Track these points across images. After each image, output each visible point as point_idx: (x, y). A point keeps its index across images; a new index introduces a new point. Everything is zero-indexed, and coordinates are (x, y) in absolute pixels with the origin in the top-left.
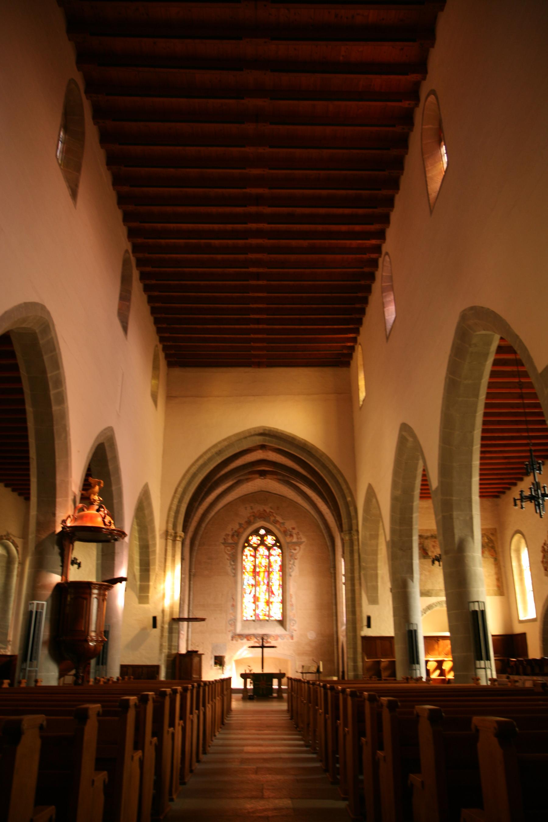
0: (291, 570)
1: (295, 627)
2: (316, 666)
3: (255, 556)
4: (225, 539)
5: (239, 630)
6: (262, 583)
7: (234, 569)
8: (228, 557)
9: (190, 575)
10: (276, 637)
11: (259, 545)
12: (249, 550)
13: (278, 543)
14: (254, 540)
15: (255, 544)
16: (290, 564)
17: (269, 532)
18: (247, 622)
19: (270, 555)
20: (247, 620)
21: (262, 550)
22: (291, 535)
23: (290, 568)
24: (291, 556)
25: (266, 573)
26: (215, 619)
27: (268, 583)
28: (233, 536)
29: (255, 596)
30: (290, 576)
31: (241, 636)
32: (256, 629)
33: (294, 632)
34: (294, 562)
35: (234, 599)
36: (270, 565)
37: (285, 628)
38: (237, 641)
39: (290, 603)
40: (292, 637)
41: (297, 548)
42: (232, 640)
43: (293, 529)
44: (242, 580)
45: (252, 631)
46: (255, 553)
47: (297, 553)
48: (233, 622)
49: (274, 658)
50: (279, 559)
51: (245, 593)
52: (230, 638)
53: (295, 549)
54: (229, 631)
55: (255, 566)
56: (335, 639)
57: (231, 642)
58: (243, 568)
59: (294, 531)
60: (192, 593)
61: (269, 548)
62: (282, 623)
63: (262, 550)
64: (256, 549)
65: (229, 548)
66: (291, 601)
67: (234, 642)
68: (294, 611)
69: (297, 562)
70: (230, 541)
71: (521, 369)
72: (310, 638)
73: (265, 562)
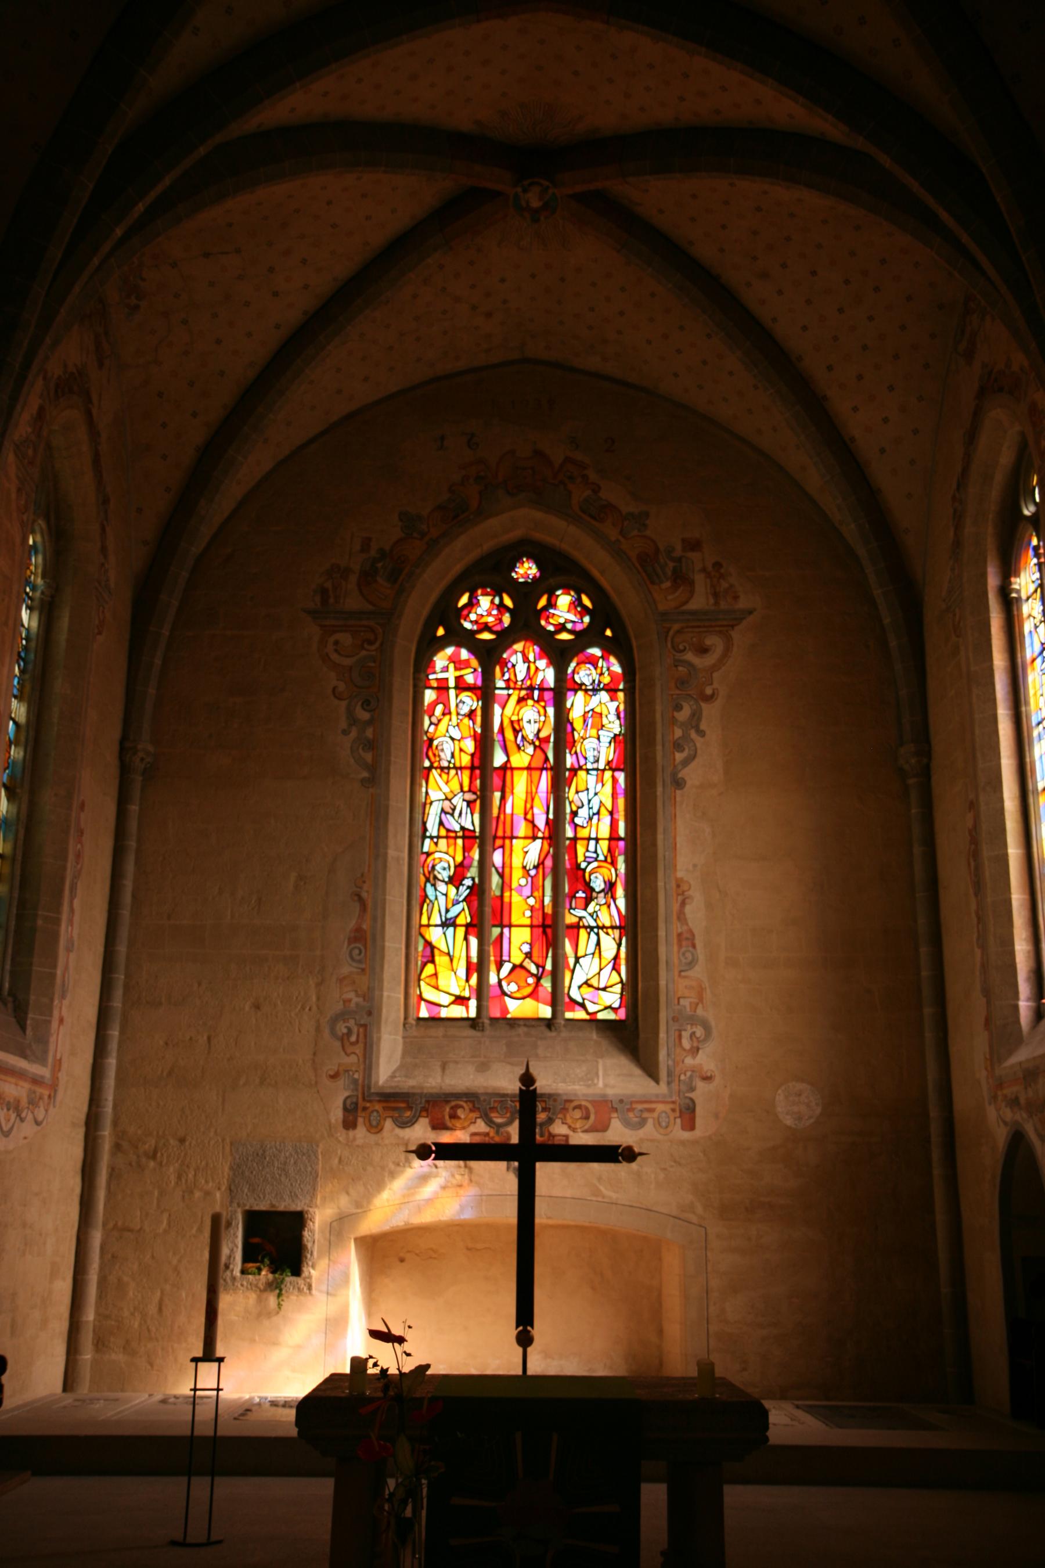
0: (679, 757)
1: (705, 1060)
2: (419, 1166)
3: (485, 693)
4: (324, 592)
5: (387, 1067)
6: (522, 829)
7: (370, 745)
8: (342, 687)
9: (125, 770)
10: (604, 1109)
11: (506, 638)
12: (459, 664)
13: (608, 627)
14: (484, 609)
15: (486, 627)
16: (674, 721)
17: (560, 571)
18: (439, 1031)
19: (564, 687)
20: (435, 1020)
21: (525, 663)
22: (681, 579)
23: (678, 746)
24: (682, 683)
25: (545, 780)
26: (257, 1007)
27: (555, 826)
28: (367, 577)
29: (478, 892)
30: (679, 784)
31: (401, 1105)
32: (483, 1067)
33: (700, 1085)
34: (696, 716)
35: (366, 902)
36: (563, 732)
37: (651, 1071)
38: (376, 1128)
39: (677, 927)
40: (688, 1115)
41: (712, 640)
42: (349, 1124)
43: (694, 545)
44: (417, 809)
45: (464, 1078)
46: (488, 677)
47: (714, 668)
48: (360, 1027)
49: (582, 1229)
50: (610, 708)
51: (432, 878)
52: (337, 1114)
53: (703, 650)
54: (334, 1076)
55: (484, 743)
56: (935, 1130)
57: (341, 1135)
58: (422, 745)
59: (694, 556)
60: (130, 867)
61: (559, 655)
62: (630, 1034)
63: (525, 663)
64: (490, 656)
65: (346, 639)
66: (681, 917)
67: (360, 1133)
68: (698, 972)
69: (710, 712)
70: (353, 602)
71: (385, 1105)
72: (789, 1121)
73: (535, 719)
